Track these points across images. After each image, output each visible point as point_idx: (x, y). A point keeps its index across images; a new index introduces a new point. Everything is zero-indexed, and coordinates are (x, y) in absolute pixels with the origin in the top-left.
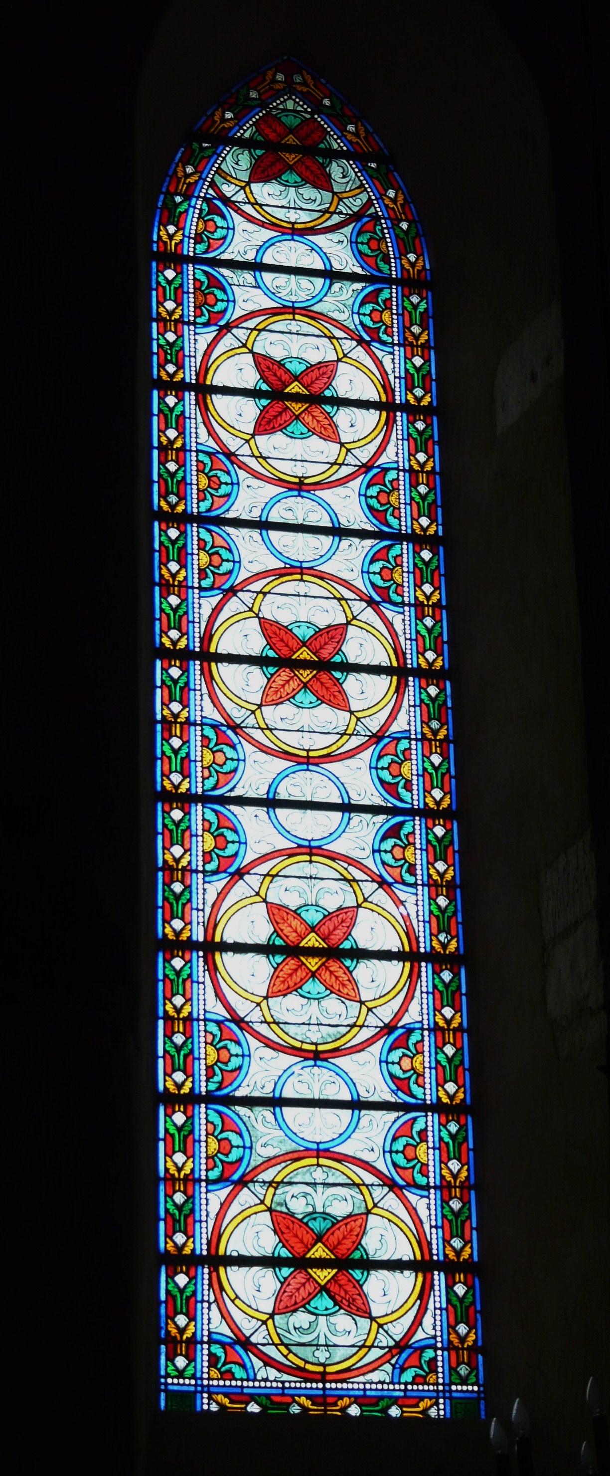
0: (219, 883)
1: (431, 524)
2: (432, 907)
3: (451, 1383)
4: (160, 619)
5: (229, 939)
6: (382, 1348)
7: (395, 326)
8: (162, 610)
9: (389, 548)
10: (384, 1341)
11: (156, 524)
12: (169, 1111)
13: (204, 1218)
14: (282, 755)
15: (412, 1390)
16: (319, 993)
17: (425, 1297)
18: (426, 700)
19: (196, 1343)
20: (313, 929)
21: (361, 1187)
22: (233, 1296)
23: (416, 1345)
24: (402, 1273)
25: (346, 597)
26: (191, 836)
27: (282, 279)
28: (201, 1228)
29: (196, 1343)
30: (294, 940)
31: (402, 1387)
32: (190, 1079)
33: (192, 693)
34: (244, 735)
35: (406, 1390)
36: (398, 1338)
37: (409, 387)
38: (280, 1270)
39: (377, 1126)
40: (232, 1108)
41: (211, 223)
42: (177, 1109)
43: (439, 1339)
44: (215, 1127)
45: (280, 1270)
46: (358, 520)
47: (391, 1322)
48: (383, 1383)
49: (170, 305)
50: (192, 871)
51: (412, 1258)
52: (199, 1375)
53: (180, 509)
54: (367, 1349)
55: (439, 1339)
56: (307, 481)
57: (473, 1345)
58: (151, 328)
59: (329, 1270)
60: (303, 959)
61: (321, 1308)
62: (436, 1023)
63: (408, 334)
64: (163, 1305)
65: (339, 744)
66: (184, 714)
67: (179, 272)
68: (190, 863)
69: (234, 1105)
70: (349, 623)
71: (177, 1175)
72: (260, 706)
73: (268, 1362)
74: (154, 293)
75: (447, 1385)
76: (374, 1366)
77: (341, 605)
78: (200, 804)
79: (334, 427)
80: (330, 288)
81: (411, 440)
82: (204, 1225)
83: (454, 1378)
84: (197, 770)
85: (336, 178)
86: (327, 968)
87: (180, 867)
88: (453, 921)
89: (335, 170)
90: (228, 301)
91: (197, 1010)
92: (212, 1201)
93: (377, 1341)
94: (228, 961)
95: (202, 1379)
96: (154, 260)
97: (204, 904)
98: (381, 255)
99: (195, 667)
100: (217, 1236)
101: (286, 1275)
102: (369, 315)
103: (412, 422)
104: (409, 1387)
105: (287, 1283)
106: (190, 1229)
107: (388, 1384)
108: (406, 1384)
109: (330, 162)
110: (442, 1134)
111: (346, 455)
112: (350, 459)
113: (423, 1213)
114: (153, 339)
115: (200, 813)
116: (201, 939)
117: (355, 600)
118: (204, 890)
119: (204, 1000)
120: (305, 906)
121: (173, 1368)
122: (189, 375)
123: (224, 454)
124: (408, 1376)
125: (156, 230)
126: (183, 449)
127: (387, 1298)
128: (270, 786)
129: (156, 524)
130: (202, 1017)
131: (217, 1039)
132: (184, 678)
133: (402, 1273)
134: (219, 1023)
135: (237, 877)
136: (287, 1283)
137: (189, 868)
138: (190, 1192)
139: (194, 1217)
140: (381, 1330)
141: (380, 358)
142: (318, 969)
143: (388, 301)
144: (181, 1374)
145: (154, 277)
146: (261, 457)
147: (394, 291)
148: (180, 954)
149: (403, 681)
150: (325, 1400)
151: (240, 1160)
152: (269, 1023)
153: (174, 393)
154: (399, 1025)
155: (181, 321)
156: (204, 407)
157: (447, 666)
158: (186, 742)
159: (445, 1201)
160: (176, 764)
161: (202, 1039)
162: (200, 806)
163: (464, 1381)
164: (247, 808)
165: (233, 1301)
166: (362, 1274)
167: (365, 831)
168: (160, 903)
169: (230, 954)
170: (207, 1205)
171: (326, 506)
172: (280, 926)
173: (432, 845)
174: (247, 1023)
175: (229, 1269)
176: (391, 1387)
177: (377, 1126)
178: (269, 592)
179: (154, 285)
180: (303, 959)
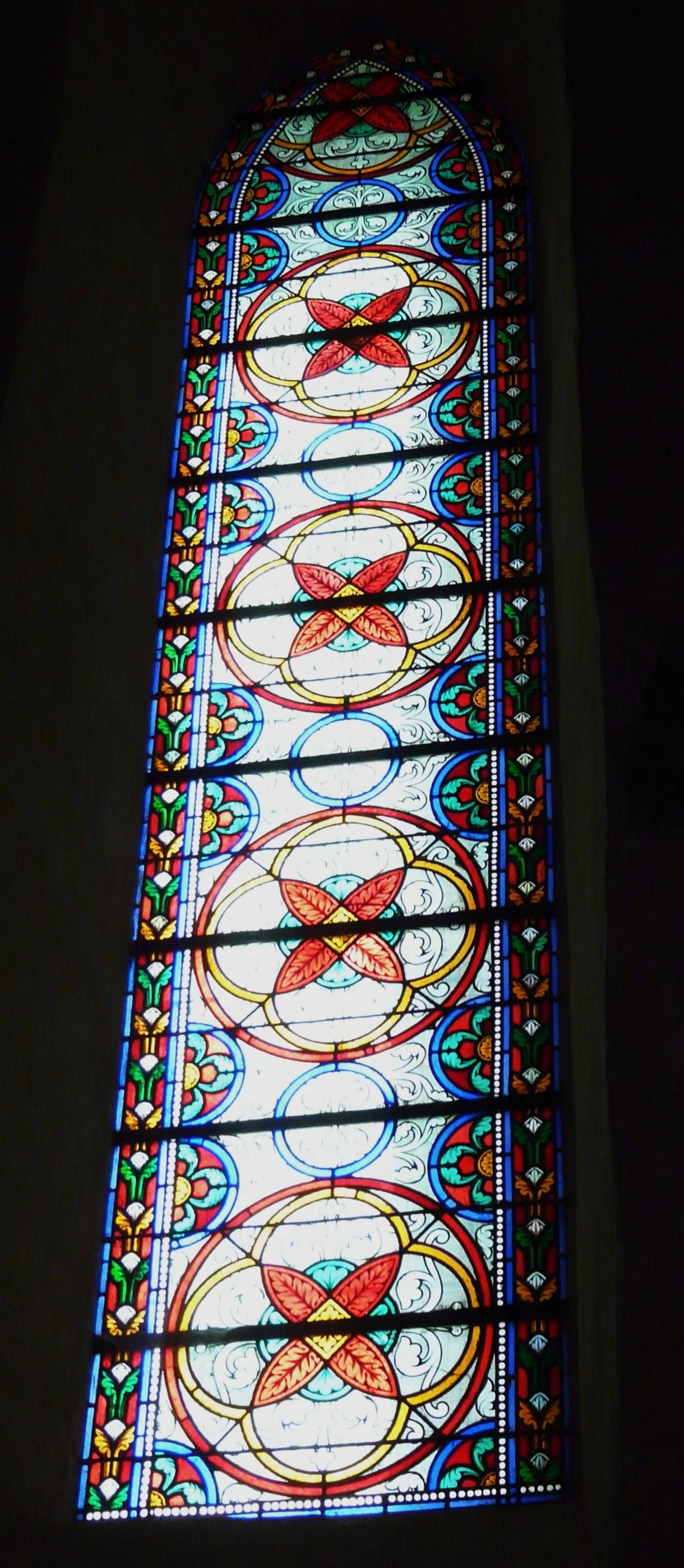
0: (194, 1244)
1: (524, 496)
2: (521, 1414)
3: (520, 1482)
4: (96, 1406)
5: (225, 929)
6: (414, 1441)
7: (500, 1272)
8: (101, 1390)
9: (465, 209)
10: (418, 1431)
11: (98, 1358)
12: (108, 1363)
13: (163, 1285)
14: (313, 708)
15: (458, 1499)
16: (333, 1391)
17: (477, 613)
18: (524, 1243)
19: (134, 1460)
20: (330, 1293)
21: (398, 840)
22: (192, 1385)
23: (467, 1433)
24: (450, 1331)
25: (401, 1210)
26: (150, 1290)
27: (346, 224)
28: (148, 1412)
29: (134, 1460)
30: (311, 919)
31: (442, 1496)
32: (160, 1110)
33: (143, 1408)
34: (281, 411)
35: (447, 1500)
36: (438, 1424)
37: (501, 357)
38: (266, 1343)
39: (418, 1139)
40: (239, 777)
41: (232, 721)
42: (179, 632)
43: (502, 1423)
44: (188, 1165)
45: (266, 1343)
46: (427, 730)
47: (430, 1401)
48: (415, 1492)
49: (144, 1109)
50: (154, 1236)
51: (460, 581)
52: (134, 1504)
53: (167, 934)
54: (388, 1446)
55: (502, 1423)
56: (345, 1047)
57: (550, 1193)
58: (157, 636)
59: (339, 1337)
60: (327, 940)
61: (326, 1391)
62: (512, 995)
63: (504, 465)
64: (126, 1045)
65: (390, 683)
66: (164, 1022)
67: (224, 243)
68: (152, 1225)
69: (241, 774)
70: (403, 1251)
71: (130, 1230)
72: (258, 1263)
73: (242, 1477)
74: (122, 1093)
75: (513, 1486)
76: (404, 1466)
77: (393, 1224)
78: (201, 781)
79: (399, 627)
80: (393, 1134)
81: (515, 1051)
82: (162, 1293)
83: (525, 1473)
84: (174, 1095)
85: (416, 118)
86: (348, 1352)
87: (169, 855)
88: (540, 780)
89: (415, 112)
90: (228, 1186)
91: (178, 1021)
92: (198, 879)
93: (407, 1430)
94: (199, 1360)
95: (138, 1509)
96: (185, 357)
97: (167, 1281)
98: (476, 808)
99: (152, 1360)
100: (180, 1304)
101: (274, 1351)
102: (453, 489)
103: (508, 601)
104: (453, 1495)
105: (274, 1363)
106: (131, 1414)
107: (421, 1493)
108: (447, 1491)
109: (409, 105)
110: (521, 1414)
111: (412, 997)
112: (420, 661)
113: (485, 1242)
114: (167, 518)
115: (173, 1153)
116: (160, 1330)
117: (420, 522)
118: (219, 563)
119: (168, 1274)
120: (321, 1261)
121: (124, 1218)
122: (156, 1324)
123: (261, 404)
124: (451, 1480)
125: (115, 1167)
126: (167, 1033)
127: (424, 1368)
128: (278, 1101)
129: (98, 1358)
130: (182, 1030)
131: (169, 1480)
132: (175, 884)
133: (450, 1331)
134: (244, 409)
135: (219, 1236)
136: (274, 1363)
137: (150, 1231)
138: (145, 1251)
139: (139, 1397)
140: (414, 1415)
141: (464, 272)
142: (334, 1355)
143: (485, 773)
144: (107, 1505)
145: (115, 1167)
146: (264, 1450)
147: (494, 758)
148: (126, 1358)
149: (480, 601)
150: (324, 1491)
151: (221, 1204)
152: (254, 1452)
153: (175, 786)
154: (456, 377)
155: (150, 1234)
156: (172, 1371)
157: (551, 898)
158: (163, 1060)
159: (513, 841)
160: (178, 664)
161: (146, 1480)
162: (173, 1145)
163: (540, 1477)
164: (278, 477)
165: (191, 1393)
166: (389, 1336)
167: (420, 475)
168: (113, 1185)
169: (246, 621)
170: (169, 1266)
171: (391, 187)
172: (280, 1296)
173: (513, 778)
174: (221, 1455)
175: (238, 622)
176: (425, 1497)
177: (418, 1139)
178: (282, 1223)
179: (122, 1081)
180: (327, 940)
